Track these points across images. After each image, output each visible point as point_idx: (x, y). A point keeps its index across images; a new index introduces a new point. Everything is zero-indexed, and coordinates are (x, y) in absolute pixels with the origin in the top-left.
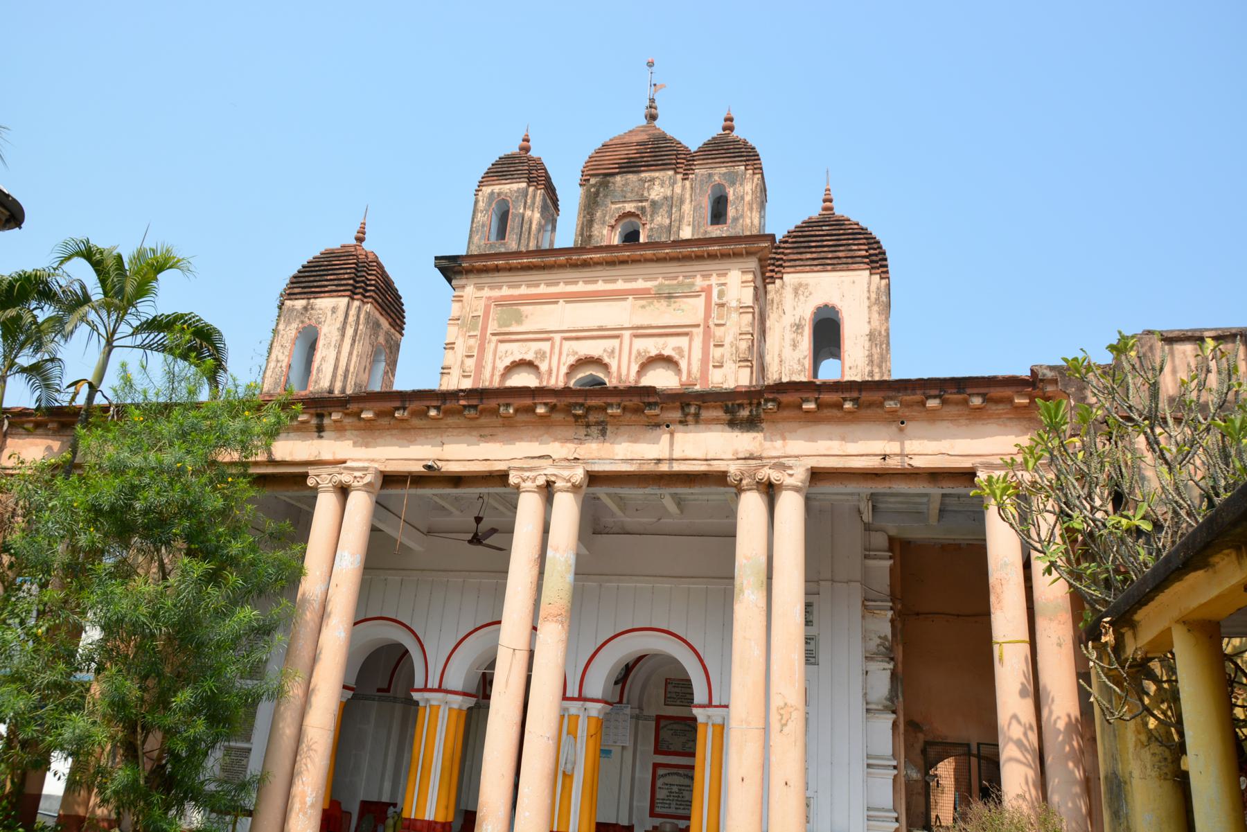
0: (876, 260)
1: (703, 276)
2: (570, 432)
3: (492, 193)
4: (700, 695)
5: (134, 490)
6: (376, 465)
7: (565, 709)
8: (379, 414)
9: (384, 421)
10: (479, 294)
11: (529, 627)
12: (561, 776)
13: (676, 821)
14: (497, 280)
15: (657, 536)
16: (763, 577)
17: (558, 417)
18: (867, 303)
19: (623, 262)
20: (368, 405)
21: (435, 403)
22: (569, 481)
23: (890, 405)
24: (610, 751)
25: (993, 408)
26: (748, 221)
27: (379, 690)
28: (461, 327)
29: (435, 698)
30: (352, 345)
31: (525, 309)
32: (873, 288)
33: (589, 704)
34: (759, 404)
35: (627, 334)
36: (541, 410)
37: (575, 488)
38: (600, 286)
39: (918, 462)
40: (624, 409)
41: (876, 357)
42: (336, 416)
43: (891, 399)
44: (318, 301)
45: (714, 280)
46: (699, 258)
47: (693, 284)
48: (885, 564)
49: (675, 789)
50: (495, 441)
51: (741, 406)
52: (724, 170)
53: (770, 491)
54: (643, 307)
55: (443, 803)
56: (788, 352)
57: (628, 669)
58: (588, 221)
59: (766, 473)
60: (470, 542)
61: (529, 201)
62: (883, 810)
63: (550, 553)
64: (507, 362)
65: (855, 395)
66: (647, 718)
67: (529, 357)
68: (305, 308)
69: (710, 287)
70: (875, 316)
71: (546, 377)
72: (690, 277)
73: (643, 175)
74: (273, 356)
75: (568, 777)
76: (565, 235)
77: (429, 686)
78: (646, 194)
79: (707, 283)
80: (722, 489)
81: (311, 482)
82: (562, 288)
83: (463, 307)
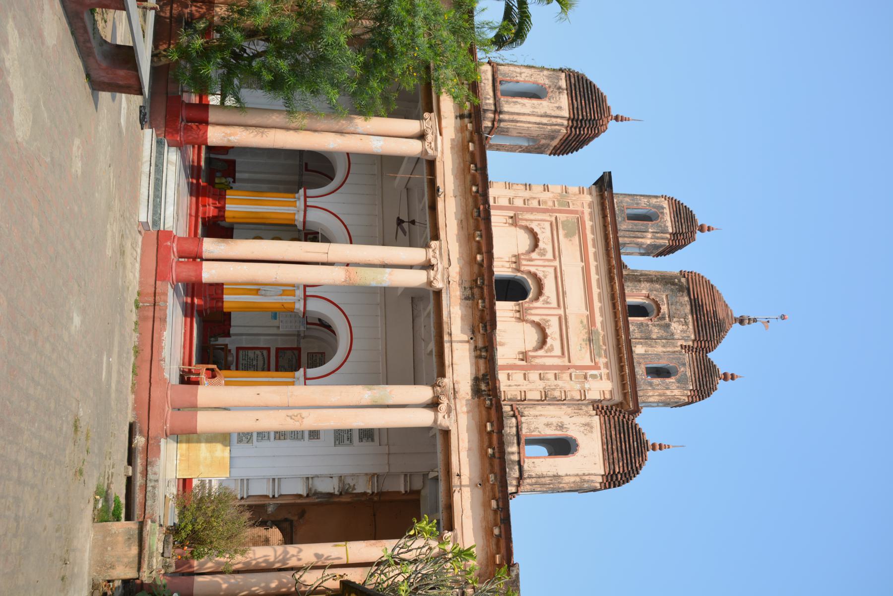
0: (613, 480)
1: (606, 364)
2: (466, 277)
3: (663, 208)
4: (311, 372)
5: (400, 24)
6: (439, 155)
7: (298, 288)
8: (472, 154)
9: (468, 158)
10: (586, 206)
11: (347, 261)
12: (256, 287)
13: (234, 363)
14: (597, 217)
15: (408, 336)
16: (380, 402)
17: (476, 268)
18: (581, 473)
19: (614, 306)
20: (477, 146)
21: (480, 189)
22: (434, 279)
23: (492, 477)
24: (275, 318)
25: (493, 541)
26: (651, 394)
27: (306, 164)
28: (561, 195)
29: (301, 204)
30: (535, 123)
31: (576, 239)
32: (592, 478)
33: (302, 302)
34: (489, 395)
35: (561, 312)
36: (479, 257)
37: (430, 283)
38: (596, 291)
39: (456, 497)
40: (483, 311)
41: (543, 480)
42: (470, 126)
43: (496, 477)
44: (566, 96)
45: (604, 371)
46: (620, 360)
47: (600, 356)
48: (401, 487)
49: (255, 363)
50: (459, 230)
51: (488, 383)
52: (689, 374)
53: (434, 405)
54: (582, 322)
55: (237, 215)
56: (543, 420)
57: (329, 327)
58: (649, 278)
59: (444, 401)
60: (398, 218)
61: (659, 235)
62: (248, 489)
63: (388, 270)
64: (536, 230)
65: (497, 455)
66: (299, 342)
67: (541, 244)
68: (560, 88)
69: (599, 368)
70: (572, 479)
71: (527, 257)
72: (605, 353)
73: (690, 317)
74: (524, 70)
75: (257, 292)
76: (634, 262)
77: (308, 199)
78: (675, 320)
79: (602, 366)
80: (435, 375)
81: (426, 115)
82: (593, 264)
83: (575, 195)
